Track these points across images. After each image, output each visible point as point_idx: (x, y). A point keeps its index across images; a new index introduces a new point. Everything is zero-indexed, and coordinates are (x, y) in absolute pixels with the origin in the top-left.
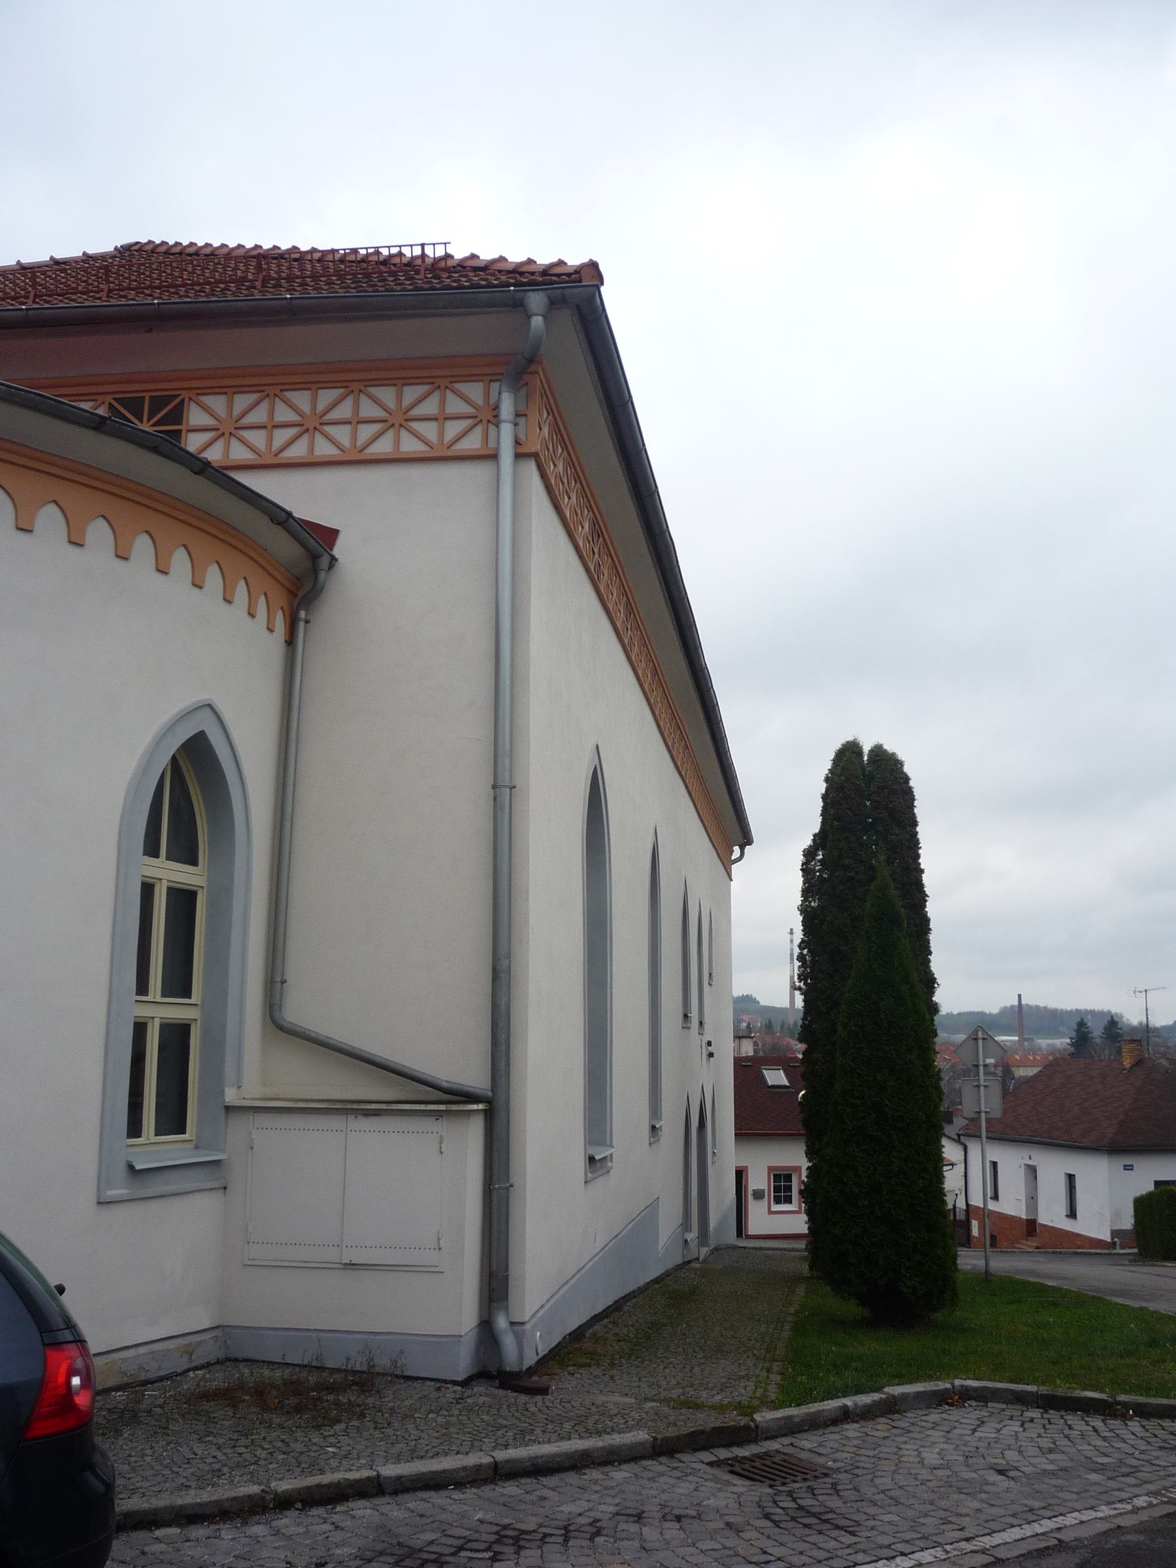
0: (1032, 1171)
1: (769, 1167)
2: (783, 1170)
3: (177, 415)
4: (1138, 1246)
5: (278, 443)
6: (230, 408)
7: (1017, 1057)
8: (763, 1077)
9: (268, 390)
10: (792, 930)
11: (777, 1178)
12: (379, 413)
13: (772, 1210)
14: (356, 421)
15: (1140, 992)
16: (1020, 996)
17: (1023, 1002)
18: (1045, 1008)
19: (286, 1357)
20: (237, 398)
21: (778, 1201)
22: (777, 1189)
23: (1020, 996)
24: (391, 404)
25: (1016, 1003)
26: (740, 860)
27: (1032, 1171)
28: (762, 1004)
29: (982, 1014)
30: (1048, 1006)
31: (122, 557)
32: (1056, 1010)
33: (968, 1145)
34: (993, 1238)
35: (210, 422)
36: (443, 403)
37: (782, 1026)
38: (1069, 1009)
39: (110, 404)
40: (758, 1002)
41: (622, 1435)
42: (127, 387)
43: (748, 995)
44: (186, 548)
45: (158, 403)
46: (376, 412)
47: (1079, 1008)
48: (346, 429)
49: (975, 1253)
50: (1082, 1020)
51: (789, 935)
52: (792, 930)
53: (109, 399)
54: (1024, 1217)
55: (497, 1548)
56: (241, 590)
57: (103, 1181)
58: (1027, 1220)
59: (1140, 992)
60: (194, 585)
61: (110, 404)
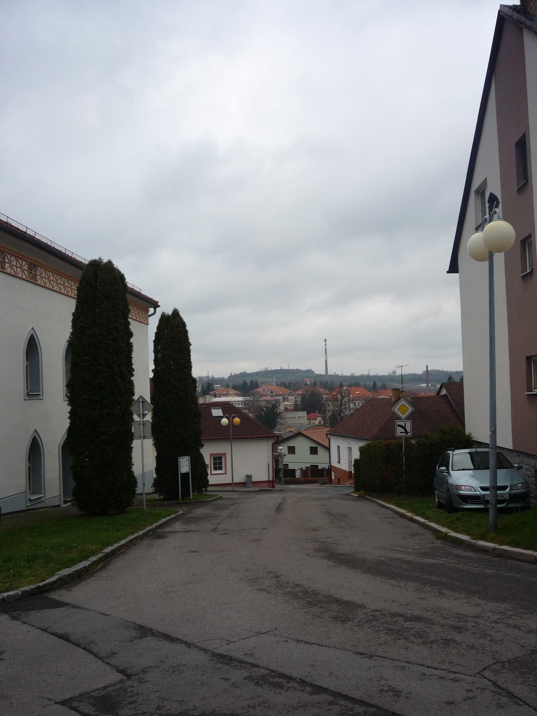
0: (350, 449)
1: (210, 454)
2: (218, 455)
4: (355, 484)
7: (423, 394)
8: (442, 395)
10: (325, 339)
11: (215, 459)
13: (212, 473)
15: (400, 367)
16: (427, 366)
17: (429, 369)
18: (443, 371)
21: (215, 469)
22: (214, 464)
23: (427, 366)
25: (426, 370)
26: (154, 314)
27: (350, 449)
28: (316, 373)
29: (415, 374)
30: (444, 370)
32: (447, 371)
33: (330, 438)
34: (338, 480)
37: (321, 383)
38: (453, 371)
40: (314, 372)
43: (309, 370)
47: (457, 371)
49: (324, 487)
50: (450, 376)
51: (324, 342)
52: (325, 339)
54: (348, 470)
58: (349, 472)
59: (400, 367)
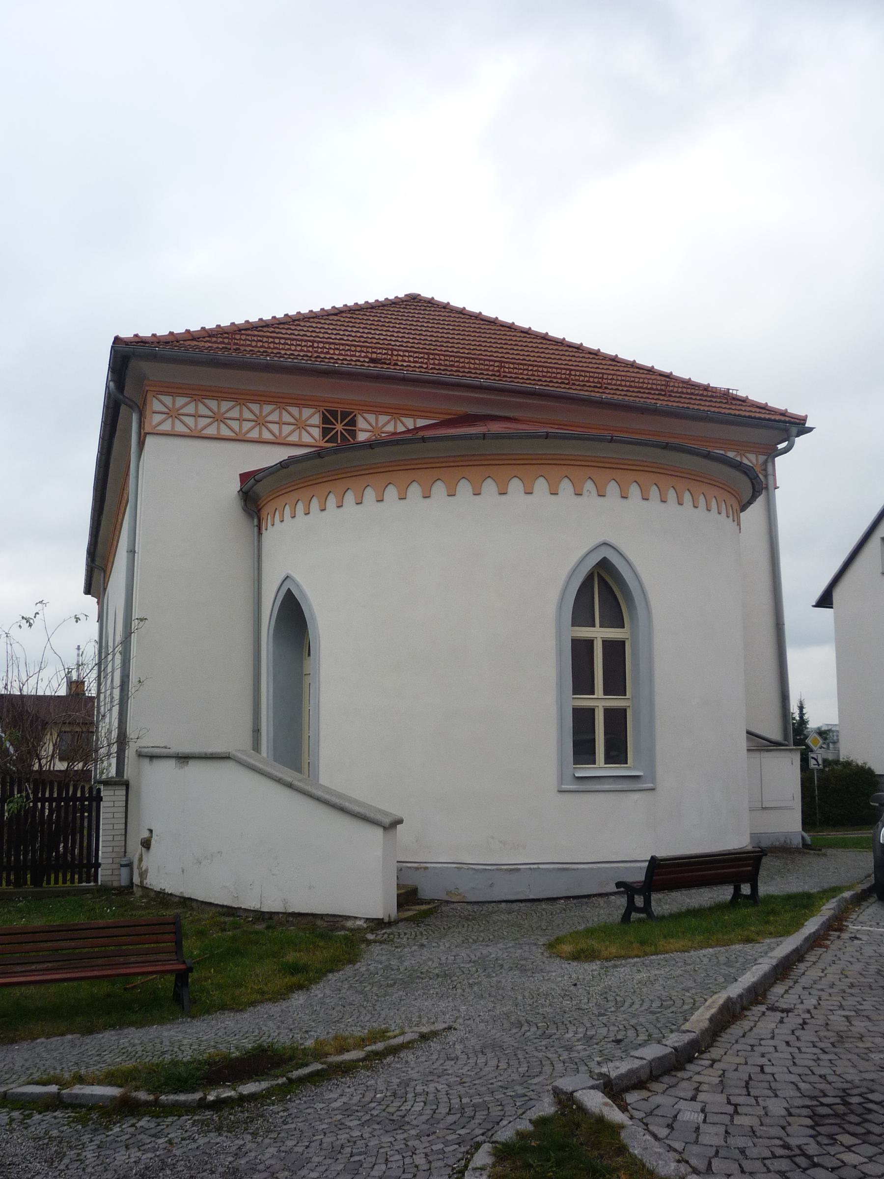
3: (353, 422)
5: (245, 429)
6: (261, 411)
9: (240, 401)
10: (79, 646)
12: (252, 417)
14: (197, 416)
19: (726, 1073)
20: (178, 399)
24: (170, 405)
31: (624, 497)
35: (253, 417)
36: (281, 414)
39: (323, 412)
41: (581, 928)
42: (330, 405)
44: (690, 491)
45: (344, 415)
46: (251, 416)
48: (277, 426)
51: (76, 650)
52: (79, 646)
53: (322, 409)
55: (822, 975)
56: (714, 503)
57: (561, 780)
60: (679, 504)
61: (323, 412)
